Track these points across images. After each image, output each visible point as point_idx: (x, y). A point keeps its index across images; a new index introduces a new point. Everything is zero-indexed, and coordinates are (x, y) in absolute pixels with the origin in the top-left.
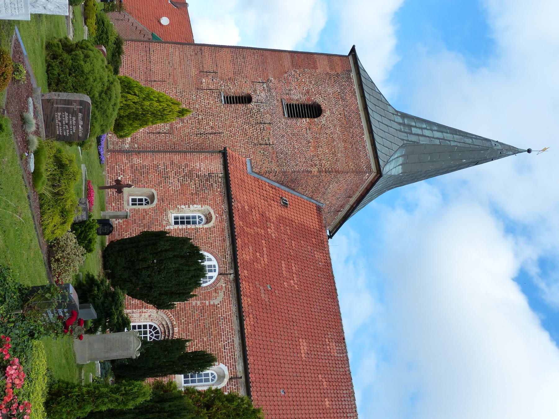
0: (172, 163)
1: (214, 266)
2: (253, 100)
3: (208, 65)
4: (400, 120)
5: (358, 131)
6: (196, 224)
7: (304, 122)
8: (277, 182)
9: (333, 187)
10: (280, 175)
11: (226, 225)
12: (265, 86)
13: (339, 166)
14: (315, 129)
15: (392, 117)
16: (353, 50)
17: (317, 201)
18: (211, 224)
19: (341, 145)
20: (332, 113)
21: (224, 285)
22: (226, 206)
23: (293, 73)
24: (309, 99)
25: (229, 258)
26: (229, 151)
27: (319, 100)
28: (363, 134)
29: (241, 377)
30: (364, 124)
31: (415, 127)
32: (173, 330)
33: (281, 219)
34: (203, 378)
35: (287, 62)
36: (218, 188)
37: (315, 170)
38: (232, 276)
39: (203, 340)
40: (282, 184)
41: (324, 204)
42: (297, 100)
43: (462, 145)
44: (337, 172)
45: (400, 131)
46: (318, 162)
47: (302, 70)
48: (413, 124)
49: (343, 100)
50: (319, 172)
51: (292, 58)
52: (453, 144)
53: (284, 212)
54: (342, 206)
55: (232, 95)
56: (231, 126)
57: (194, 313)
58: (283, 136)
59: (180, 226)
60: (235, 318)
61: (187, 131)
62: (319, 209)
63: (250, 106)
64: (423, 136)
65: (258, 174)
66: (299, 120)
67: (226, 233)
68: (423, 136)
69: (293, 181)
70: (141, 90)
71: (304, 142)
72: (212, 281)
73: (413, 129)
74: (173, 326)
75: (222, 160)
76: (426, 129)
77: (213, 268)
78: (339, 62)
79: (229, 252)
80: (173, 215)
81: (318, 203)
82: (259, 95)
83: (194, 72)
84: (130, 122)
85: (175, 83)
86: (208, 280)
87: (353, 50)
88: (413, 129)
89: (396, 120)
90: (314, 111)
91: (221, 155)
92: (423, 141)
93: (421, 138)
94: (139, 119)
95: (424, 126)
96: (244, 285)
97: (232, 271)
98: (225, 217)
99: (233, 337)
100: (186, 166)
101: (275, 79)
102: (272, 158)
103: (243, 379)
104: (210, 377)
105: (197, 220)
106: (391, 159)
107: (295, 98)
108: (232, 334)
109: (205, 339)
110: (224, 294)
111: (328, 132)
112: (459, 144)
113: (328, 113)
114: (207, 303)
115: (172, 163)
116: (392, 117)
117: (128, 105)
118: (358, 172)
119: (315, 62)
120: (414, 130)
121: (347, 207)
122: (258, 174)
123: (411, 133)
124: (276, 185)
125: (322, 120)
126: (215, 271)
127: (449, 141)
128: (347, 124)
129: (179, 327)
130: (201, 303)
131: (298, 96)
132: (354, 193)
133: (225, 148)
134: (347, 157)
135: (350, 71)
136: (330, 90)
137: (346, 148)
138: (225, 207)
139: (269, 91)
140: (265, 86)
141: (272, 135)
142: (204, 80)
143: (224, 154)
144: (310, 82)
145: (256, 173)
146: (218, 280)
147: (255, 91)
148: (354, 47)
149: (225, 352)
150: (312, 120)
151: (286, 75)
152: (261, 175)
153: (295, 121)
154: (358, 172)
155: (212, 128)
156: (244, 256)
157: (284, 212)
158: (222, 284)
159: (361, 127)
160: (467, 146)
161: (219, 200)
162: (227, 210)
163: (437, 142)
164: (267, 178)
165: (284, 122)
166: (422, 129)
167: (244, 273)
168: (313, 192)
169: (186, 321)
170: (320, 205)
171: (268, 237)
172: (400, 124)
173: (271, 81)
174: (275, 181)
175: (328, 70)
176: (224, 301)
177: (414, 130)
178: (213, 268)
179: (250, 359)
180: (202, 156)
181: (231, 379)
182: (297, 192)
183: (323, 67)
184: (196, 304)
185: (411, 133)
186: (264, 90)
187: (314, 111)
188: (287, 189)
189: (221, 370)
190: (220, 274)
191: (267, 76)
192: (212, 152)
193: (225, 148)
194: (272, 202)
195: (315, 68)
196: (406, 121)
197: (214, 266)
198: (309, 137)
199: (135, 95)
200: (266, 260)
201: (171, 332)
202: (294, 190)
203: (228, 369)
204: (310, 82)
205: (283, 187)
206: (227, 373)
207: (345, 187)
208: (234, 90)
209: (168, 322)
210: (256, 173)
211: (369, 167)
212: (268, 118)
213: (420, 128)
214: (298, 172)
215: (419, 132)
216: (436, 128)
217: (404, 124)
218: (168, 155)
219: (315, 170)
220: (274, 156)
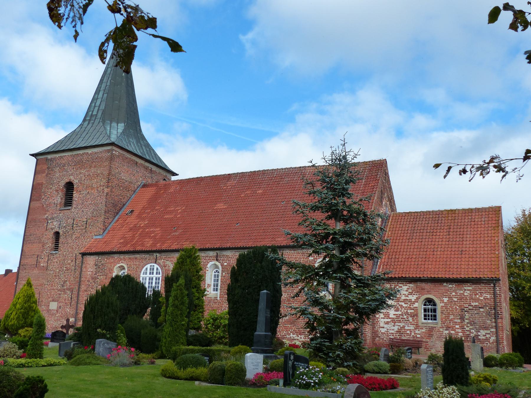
0: (86, 291)
1: (151, 266)
2: (58, 230)
3: (33, 261)
4: (87, 123)
5: (85, 156)
7: (75, 195)
8: (115, 217)
9: (124, 176)
10: (108, 215)
11: (127, 256)
12: (49, 221)
13: (106, 173)
14: (80, 188)
15: (83, 129)
16: (32, 155)
17: (138, 187)
18: (126, 266)
19: (93, 170)
20: (72, 175)
22: (116, 255)
23: (44, 200)
24: (62, 191)
25: (147, 256)
26: (83, 250)
27: (63, 183)
28: (88, 153)
30: (81, 152)
31: (93, 111)
33: (139, 217)
35: (36, 204)
36: (104, 260)
37: (106, 190)
38: (157, 254)
40: (117, 213)
41: (141, 181)
42: (62, 199)
43: (110, 76)
44: (109, 174)
45: (93, 123)
46: (102, 188)
47: (42, 194)
48: (91, 113)
49: (64, 166)
50: (108, 187)
51: (34, 200)
52: (108, 84)
53: (136, 213)
54: (146, 168)
55: (53, 245)
56: (71, 247)
58: (83, 211)
59: (219, 287)
61: (72, 279)
62: (145, 186)
63: (61, 233)
64: (99, 106)
65: (105, 231)
66: (74, 198)
67: (132, 256)
68: (99, 106)
69: (115, 205)
70: (10, 310)
71: (88, 196)
72: (159, 268)
73: (94, 114)
75: (88, 256)
76: (95, 103)
78: (41, 166)
79: (143, 256)
80: (212, 292)
81: (141, 186)
82: (55, 225)
83: (36, 271)
84: (30, 317)
85: (41, 285)
87: (32, 155)
88: (94, 114)
89: (86, 126)
90: (70, 186)
91: (85, 257)
92: (103, 107)
93: (101, 108)
94: (28, 311)
95: (93, 104)
96: (164, 247)
97: (155, 254)
98: (122, 256)
100: (88, 281)
101: (46, 214)
102: (96, 220)
103: (218, 252)
104: (216, 274)
105: (216, 274)
106: (108, 132)
107: (59, 200)
111: (83, 178)
112: (110, 79)
113: (71, 177)
115: (86, 291)
116: (83, 129)
117: (17, 318)
118: (112, 158)
119: (39, 184)
120: (95, 113)
121: (147, 164)
122: (104, 231)
123: (96, 115)
124: (117, 218)
125: (75, 182)
126: (154, 266)
127: (106, 86)
128: (80, 164)
131: (59, 199)
132: (132, 160)
133: (80, 254)
134: (100, 166)
135: (47, 159)
136: (57, 175)
137: (95, 167)
138: (116, 256)
139: (53, 218)
140: (49, 221)
141: (81, 219)
142: (42, 265)
143: (84, 254)
144: (51, 188)
145: (103, 232)
146: (159, 264)
147: (52, 229)
148: (30, 155)
150: (75, 189)
151: (45, 206)
152: (106, 229)
153: (74, 202)
154: (112, 158)
155: (72, 261)
156: (148, 244)
157: (136, 213)
158: (161, 262)
159: (83, 154)
160: (112, 72)
161: (112, 260)
162: (118, 255)
163: (105, 95)
164: (109, 224)
165: (74, 210)
166: (95, 106)
167: (158, 246)
168: (128, 191)
170: (142, 184)
171: (147, 226)
172: (89, 123)
173: (47, 217)
174: (114, 219)
175: (44, 175)
177: (95, 113)
179: (208, 246)
180: (84, 270)
181: (217, 260)
182: (126, 203)
183: (42, 178)
185: (96, 115)
186: (52, 222)
187: (70, 186)
188: (123, 210)
190: (156, 263)
191: (43, 219)
192: (82, 262)
193: (80, 254)
194: (127, 221)
195: (42, 184)
196: (88, 118)
197: (151, 266)
198: (85, 192)
199: (12, 313)
200: (157, 230)
202: (124, 205)
204: (51, 188)
205: (120, 213)
206: (213, 263)
207: (125, 167)
208: (50, 244)
210: (103, 232)
211: (108, 151)
212: (70, 221)
213: (94, 108)
214: (106, 202)
215: (96, 108)
216: (96, 96)
217: (90, 120)
218: (81, 293)
219: (106, 190)
220: (94, 218)
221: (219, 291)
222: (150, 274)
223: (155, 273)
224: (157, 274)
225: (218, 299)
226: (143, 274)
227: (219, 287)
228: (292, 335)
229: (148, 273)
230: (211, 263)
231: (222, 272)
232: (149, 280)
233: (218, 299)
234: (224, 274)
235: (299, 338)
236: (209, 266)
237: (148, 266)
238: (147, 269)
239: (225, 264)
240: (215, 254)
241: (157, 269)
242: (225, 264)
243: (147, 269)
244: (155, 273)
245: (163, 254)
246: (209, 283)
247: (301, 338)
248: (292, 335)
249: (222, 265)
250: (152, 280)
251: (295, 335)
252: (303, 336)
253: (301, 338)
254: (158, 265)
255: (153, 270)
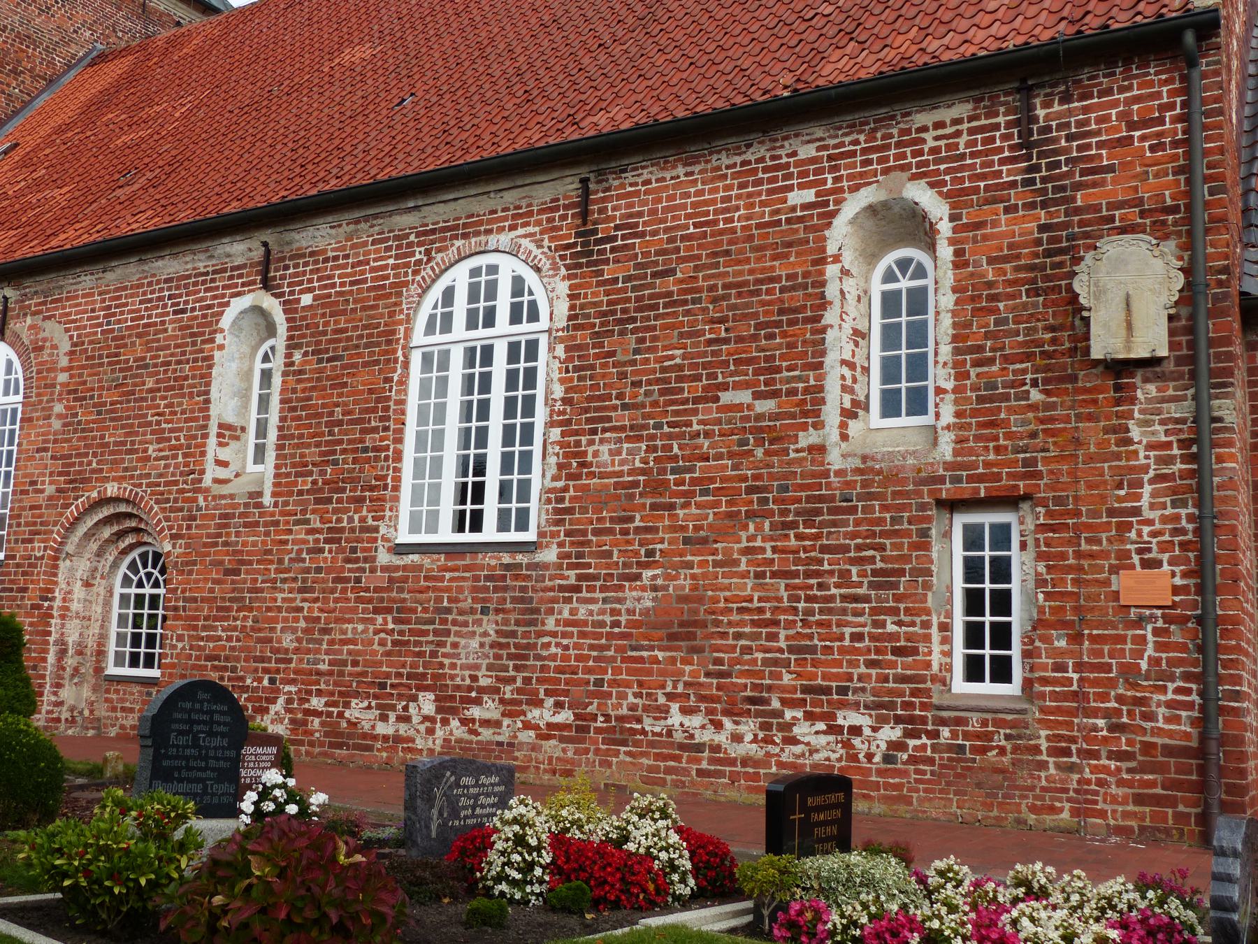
1: (475, 272)
6: (924, 290)
21: (29, 320)
29: (265, 244)
32: (116, 500)
34: (904, 319)
39: (151, 391)
57: (79, 423)
59: (939, 376)
60: (110, 276)
72: (531, 279)
74: (104, 501)
77: (483, 279)
86: (526, 298)
99: (158, 282)
103: (268, 236)
105: (904, 284)
108: (150, 284)
109: (150, 383)
110: (49, 318)
114: (63, 377)
126: (493, 269)
129: (106, 479)
130: (60, 400)
149: (193, 309)
169: (95, 454)
176: (65, 319)
178: (483, 279)
181: (267, 285)
184: (59, 416)
189: (245, 323)
197: (475, 272)
201: (123, 508)
203: (238, 294)
206: (245, 301)
209: (96, 519)
221: (271, 455)
222: (471, 324)
223: (503, 314)
224: (515, 318)
225: (267, 500)
226: (430, 330)
227: (939, 376)
228: (675, 718)
229: (459, 319)
230: (239, 305)
231: (292, 346)
232: (470, 362)
233: (267, 500)
234: (297, 356)
235: (722, 738)
236: (226, 321)
237: (459, 276)
238: (448, 295)
239: (307, 299)
240: (258, 254)
241: (518, 286)
242: (307, 299)
243: (448, 295)
244: (503, 314)
245: (31, 285)
246: (230, 419)
247: (737, 738)
248: (675, 718)
249: (290, 307)
250: (444, 365)
251: (696, 721)
252: (748, 728)
253: (737, 738)
254: (12, 345)
255: (492, 293)
